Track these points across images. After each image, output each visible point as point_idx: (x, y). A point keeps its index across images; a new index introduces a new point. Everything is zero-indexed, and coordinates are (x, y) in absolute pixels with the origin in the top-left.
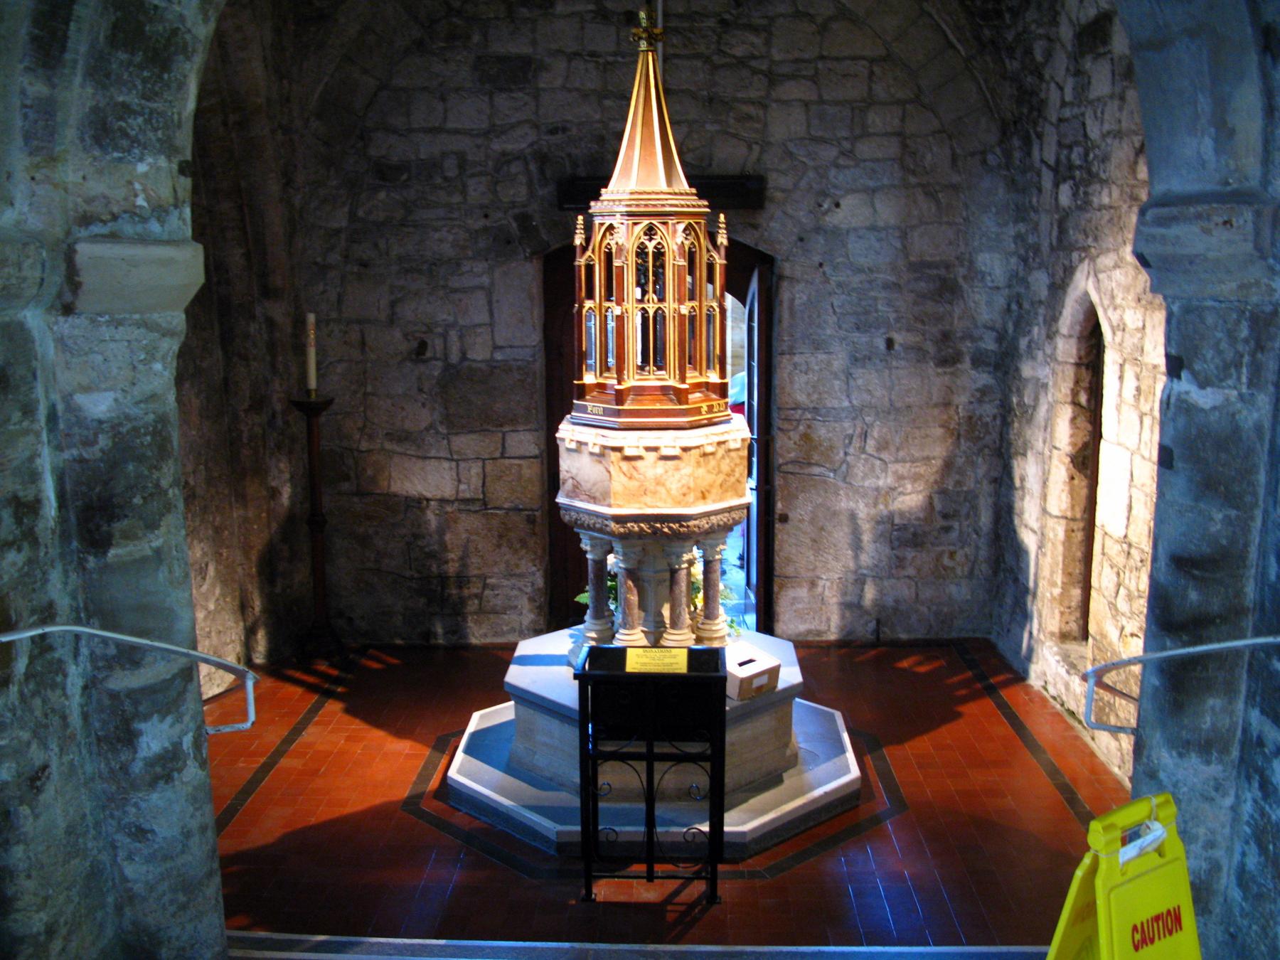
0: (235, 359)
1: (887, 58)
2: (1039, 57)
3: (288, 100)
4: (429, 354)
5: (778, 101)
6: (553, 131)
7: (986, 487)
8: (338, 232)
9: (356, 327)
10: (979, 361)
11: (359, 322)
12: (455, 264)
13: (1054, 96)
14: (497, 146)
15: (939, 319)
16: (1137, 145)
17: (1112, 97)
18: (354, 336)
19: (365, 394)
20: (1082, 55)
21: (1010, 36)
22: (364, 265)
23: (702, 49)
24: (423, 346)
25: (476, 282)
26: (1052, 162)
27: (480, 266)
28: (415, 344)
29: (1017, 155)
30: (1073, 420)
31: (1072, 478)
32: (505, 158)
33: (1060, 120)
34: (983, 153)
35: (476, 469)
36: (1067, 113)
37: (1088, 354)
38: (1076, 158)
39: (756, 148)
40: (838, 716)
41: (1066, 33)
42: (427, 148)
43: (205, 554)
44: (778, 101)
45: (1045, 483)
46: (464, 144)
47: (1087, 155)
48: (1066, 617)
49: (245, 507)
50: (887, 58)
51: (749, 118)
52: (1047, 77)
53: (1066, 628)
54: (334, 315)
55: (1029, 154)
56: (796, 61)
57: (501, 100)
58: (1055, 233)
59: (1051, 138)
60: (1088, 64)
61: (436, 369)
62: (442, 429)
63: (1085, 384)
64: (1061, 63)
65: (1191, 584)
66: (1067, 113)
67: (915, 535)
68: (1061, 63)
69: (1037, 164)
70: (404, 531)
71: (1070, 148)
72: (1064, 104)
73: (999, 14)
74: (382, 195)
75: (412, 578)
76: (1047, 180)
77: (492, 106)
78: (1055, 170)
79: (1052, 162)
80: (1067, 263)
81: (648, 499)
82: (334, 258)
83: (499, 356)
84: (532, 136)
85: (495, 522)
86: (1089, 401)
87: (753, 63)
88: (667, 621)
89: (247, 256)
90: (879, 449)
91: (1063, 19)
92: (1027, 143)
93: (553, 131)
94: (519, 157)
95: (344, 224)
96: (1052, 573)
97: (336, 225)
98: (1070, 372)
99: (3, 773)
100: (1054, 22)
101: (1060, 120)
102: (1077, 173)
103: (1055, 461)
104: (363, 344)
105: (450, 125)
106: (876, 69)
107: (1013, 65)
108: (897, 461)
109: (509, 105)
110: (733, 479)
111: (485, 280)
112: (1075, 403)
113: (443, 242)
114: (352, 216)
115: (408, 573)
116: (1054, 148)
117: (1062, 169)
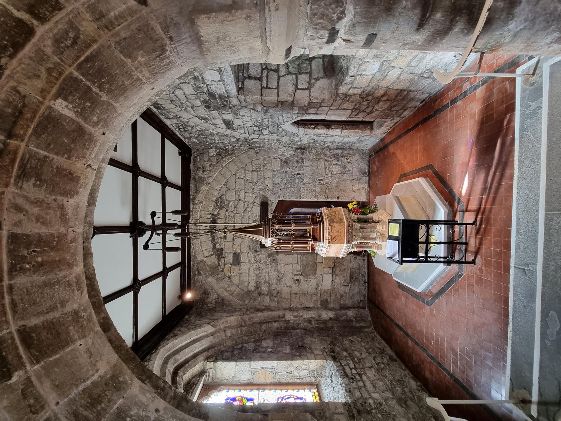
0: (299, 327)
1: (235, 175)
2: (235, 139)
3: (240, 309)
4: (299, 279)
5: (244, 199)
6: (250, 249)
7: (332, 151)
8: (270, 298)
9: (292, 295)
10: (303, 154)
11: (291, 294)
12: (279, 272)
13: (243, 135)
14: (253, 261)
15: (293, 163)
16: (253, 111)
17: (242, 119)
18: (294, 296)
19: (307, 294)
20: (233, 128)
21: (231, 147)
22: (278, 293)
23: (233, 215)
24: (297, 280)
25: (283, 267)
26: (258, 136)
27: (279, 266)
28: (296, 282)
29: (257, 145)
30: (319, 129)
31: (332, 129)
32: (256, 261)
33: (248, 134)
34: (256, 153)
35: (325, 269)
36: (247, 132)
37: (303, 126)
38: (257, 129)
39: (255, 204)
40: (395, 185)
41: (229, 132)
42: (252, 276)
43: (346, 340)
44: (244, 199)
45: (333, 136)
46: (252, 269)
47: (256, 126)
48: (367, 129)
49: (334, 327)
50: (235, 175)
51: (248, 205)
52: (239, 137)
53: (370, 128)
54: (289, 300)
55: (256, 142)
56: (236, 194)
57: (242, 260)
58: (274, 135)
59: (252, 136)
60: (235, 126)
61: (302, 277)
62: (316, 276)
63: (310, 126)
64: (236, 134)
65: (432, 17)
66: (247, 132)
67: (342, 168)
68: (236, 134)
69: (259, 140)
70: (339, 287)
71: (254, 131)
72: (245, 133)
73: (226, 149)
74: (262, 288)
75: (351, 285)
76: (262, 137)
77: (244, 263)
78: (260, 135)
79: (258, 136)
80: (281, 131)
81: (342, 235)
82: (276, 299)
83: (299, 263)
84: (251, 253)
85: (338, 265)
86: (313, 125)
87: (236, 204)
88: (42, 100)
89: (275, 321)
90: (323, 176)
91: (226, 133)
92: (253, 142)
93: (250, 249)
94: (255, 256)
95: (269, 297)
96: (355, 133)
97: (269, 299)
98: (307, 130)
99: (419, 420)
100: (226, 136)
101: (248, 134)
102: (260, 129)
103: (328, 133)
104: (296, 294)
105: (248, 272)
106: (238, 177)
107: (237, 146)
108: (325, 172)
109: (244, 258)
110: (336, 212)
111: (282, 265)
112: (314, 128)
113: (274, 275)
114: (267, 295)
115: (350, 286)
116: (255, 135)
117: (259, 133)
